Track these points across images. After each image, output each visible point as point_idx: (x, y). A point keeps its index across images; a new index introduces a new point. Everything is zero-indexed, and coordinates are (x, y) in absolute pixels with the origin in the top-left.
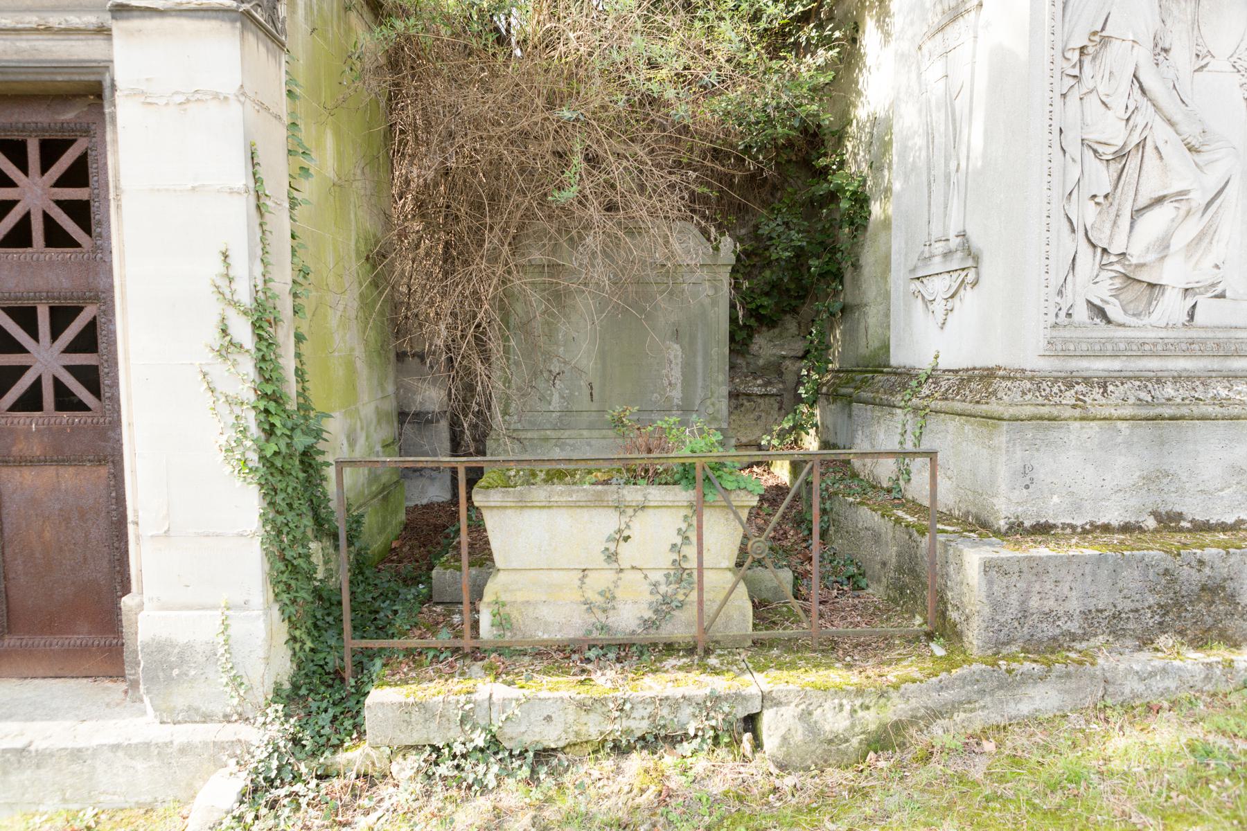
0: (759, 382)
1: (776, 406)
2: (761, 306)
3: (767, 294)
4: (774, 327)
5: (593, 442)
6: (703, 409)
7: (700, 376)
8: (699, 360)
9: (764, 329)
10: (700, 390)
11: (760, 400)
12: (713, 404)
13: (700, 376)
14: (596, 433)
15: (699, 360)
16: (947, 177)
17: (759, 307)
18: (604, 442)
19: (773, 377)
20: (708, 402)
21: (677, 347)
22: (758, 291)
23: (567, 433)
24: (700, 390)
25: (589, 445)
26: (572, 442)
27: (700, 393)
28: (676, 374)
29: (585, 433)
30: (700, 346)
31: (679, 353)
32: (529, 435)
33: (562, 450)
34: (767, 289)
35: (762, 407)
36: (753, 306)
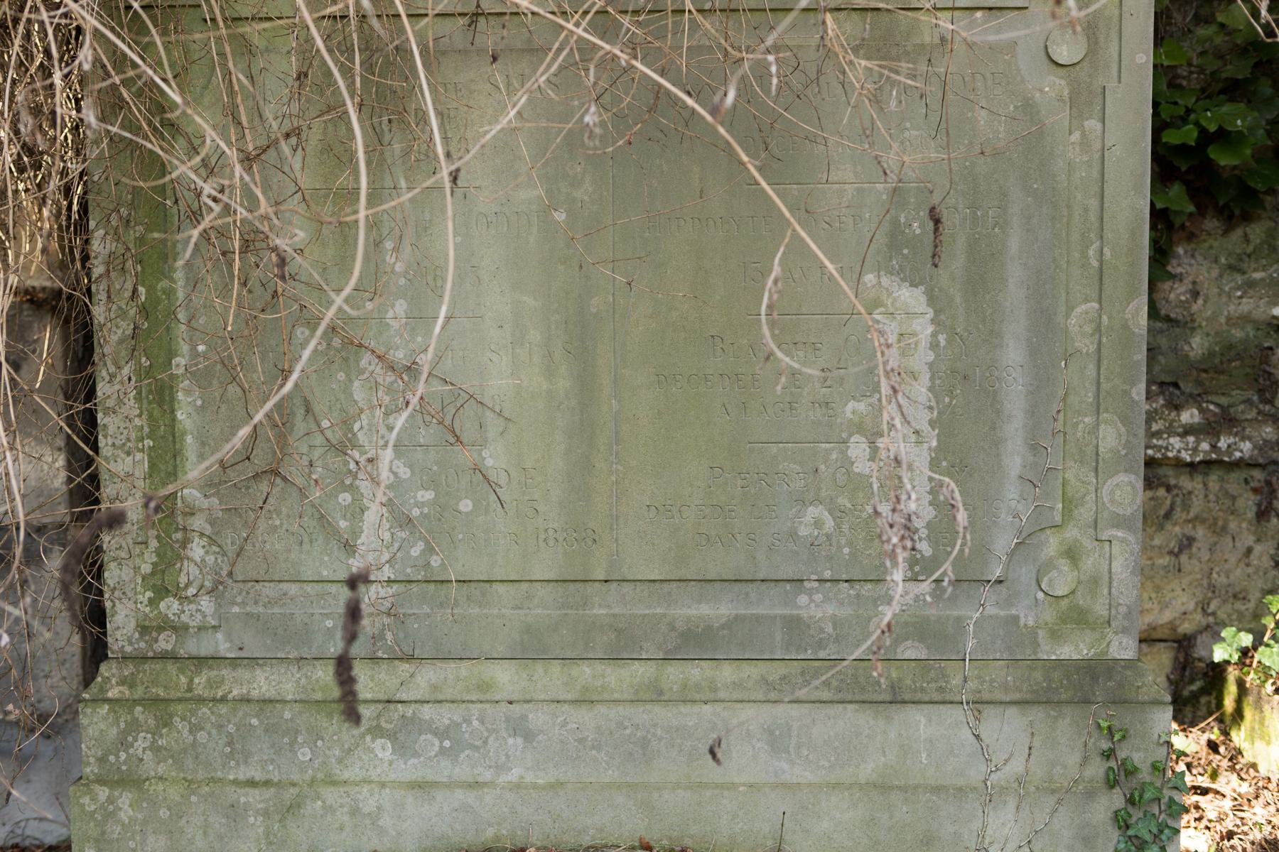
0: (1189, 416)
1: (1248, 503)
2: (1222, 136)
3: (1233, 90)
4: (1247, 218)
5: (538, 718)
6: (1025, 574)
7: (1014, 430)
8: (1013, 355)
9: (1211, 224)
10: (1012, 492)
11: (1186, 483)
12: (1072, 554)
13: (1014, 430)
14: (550, 679)
15: (1013, 355)
16: (164, 511)
17: (1206, 138)
18: (586, 718)
19: (1239, 399)
20: (1052, 545)
21: (911, 297)
22: (1195, 82)
23: (427, 677)
24: (1012, 492)
25: (519, 728)
26: (444, 716)
27: (1013, 501)
28: (908, 439)
29: (505, 677)
30: (1014, 293)
31: (924, 329)
32: (262, 683)
33: (402, 750)
34: (1237, 70)
35: (1197, 505)
36: (1188, 135)
